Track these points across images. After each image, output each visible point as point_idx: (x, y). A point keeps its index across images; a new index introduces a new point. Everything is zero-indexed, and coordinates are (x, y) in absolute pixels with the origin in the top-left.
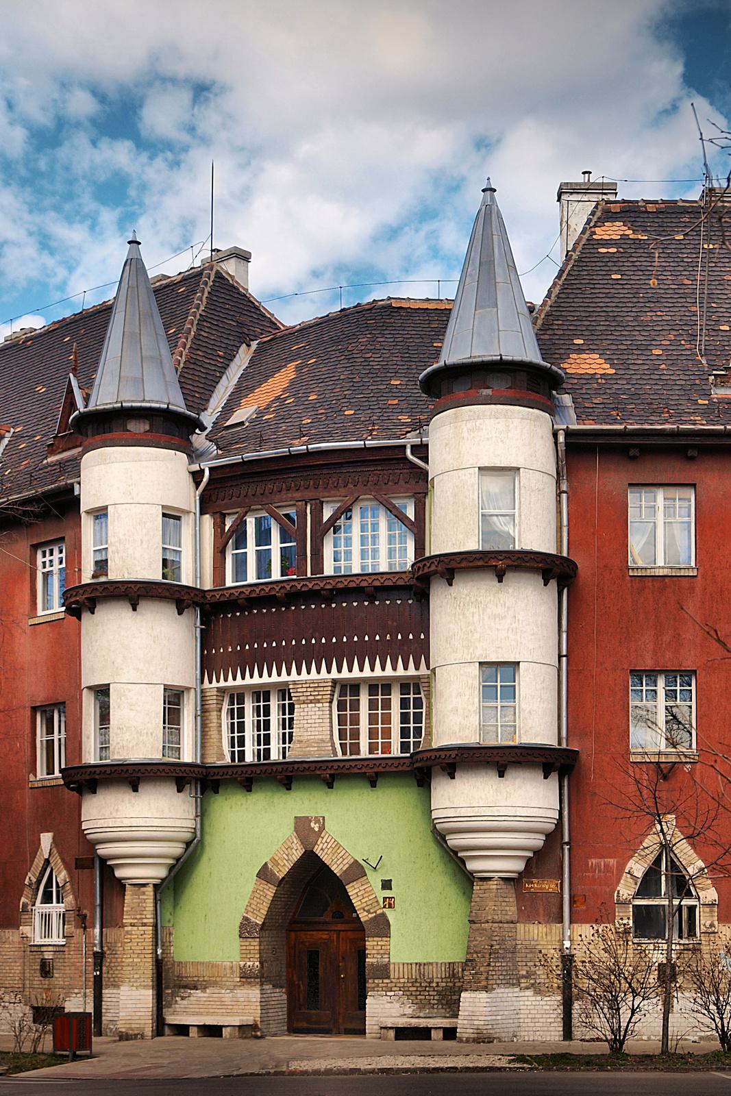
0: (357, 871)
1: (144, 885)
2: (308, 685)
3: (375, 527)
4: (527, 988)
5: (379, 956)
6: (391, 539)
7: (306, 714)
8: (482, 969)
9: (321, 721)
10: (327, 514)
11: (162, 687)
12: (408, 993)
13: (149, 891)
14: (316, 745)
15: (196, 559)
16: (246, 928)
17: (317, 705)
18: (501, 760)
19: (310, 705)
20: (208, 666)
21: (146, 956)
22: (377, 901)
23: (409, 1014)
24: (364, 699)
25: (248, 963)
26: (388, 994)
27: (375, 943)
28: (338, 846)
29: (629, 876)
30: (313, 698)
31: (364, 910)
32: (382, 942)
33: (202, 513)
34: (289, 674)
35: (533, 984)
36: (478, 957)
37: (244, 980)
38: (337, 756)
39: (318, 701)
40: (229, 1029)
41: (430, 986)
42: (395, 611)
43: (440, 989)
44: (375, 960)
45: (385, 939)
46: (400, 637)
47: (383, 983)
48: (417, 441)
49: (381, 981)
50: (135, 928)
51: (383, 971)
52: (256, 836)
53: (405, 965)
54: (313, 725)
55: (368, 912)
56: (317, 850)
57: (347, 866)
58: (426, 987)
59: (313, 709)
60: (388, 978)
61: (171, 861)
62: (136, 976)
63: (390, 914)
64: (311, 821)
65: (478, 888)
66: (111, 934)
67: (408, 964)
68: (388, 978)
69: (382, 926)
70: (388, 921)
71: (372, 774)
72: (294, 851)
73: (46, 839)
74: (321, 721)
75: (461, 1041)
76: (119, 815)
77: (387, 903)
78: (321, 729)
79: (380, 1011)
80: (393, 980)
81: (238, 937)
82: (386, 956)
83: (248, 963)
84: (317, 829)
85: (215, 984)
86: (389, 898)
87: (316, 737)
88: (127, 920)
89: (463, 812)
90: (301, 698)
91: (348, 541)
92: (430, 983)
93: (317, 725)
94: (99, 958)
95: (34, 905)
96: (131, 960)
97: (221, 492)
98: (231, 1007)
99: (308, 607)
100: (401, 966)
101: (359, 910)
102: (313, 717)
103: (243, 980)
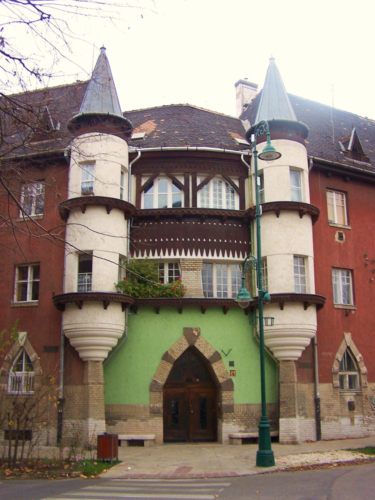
0: (217, 356)
1: (98, 361)
2: (190, 261)
3: (220, 191)
4: (302, 415)
5: (229, 401)
6: (227, 197)
7: (188, 275)
8: (291, 406)
9: (196, 279)
10: (198, 183)
11: (293, 256)
12: (243, 420)
13: (101, 364)
14: (194, 291)
15: (128, 194)
16: (153, 387)
17: (194, 271)
18: (302, 300)
19: (190, 271)
20: (133, 248)
21: (101, 401)
22: (227, 373)
23: (244, 431)
24: (166, 270)
25: (156, 405)
26: (234, 420)
27: (227, 394)
28: (208, 343)
29: (337, 360)
30: (192, 268)
31: (221, 377)
32: (230, 393)
33: (132, 174)
34: (180, 254)
35: (304, 413)
36: (287, 400)
37: (153, 414)
38: (213, 296)
39: (195, 270)
40: (148, 442)
41: (252, 416)
42: (238, 230)
43: (257, 417)
44: (226, 403)
45: (231, 392)
46: (236, 242)
47: (96, 386)
48: (247, 154)
49: (230, 414)
50: (94, 385)
51: (231, 408)
52: (164, 335)
53: (241, 406)
54: (192, 281)
55: (223, 378)
56: (196, 345)
57: (212, 354)
58: (251, 416)
59: (192, 273)
60: (233, 412)
61: (111, 349)
62: (97, 412)
63: (234, 379)
64: (193, 330)
65: (283, 365)
66: (72, 389)
67: (242, 405)
68: (233, 412)
69: (230, 385)
70: (233, 383)
71: (225, 306)
72: (183, 346)
73: (22, 335)
74: (196, 279)
75: (283, 444)
76: (74, 322)
77: (232, 373)
78: (196, 283)
79: (229, 429)
80: (236, 413)
81: (149, 391)
82: (232, 401)
83: (156, 405)
84: (196, 334)
85: (133, 417)
86: (233, 371)
87: (195, 288)
88: (90, 381)
89: (288, 327)
90: (186, 268)
91: (208, 195)
92: (252, 414)
93: (194, 281)
94: (62, 402)
95: (9, 372)
96: (93, 403)
97: (146, 166)
98: (144, 429)
99: (164, 223)
100: (239, 406)
101: (219, 377)
102: (192, 277)
103: (152, 414)
